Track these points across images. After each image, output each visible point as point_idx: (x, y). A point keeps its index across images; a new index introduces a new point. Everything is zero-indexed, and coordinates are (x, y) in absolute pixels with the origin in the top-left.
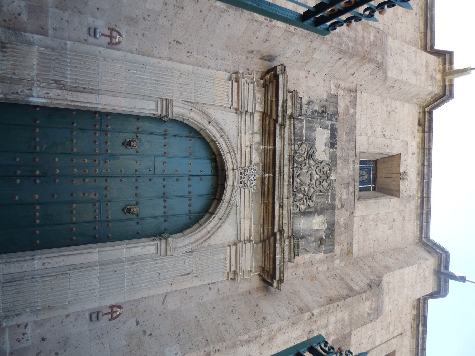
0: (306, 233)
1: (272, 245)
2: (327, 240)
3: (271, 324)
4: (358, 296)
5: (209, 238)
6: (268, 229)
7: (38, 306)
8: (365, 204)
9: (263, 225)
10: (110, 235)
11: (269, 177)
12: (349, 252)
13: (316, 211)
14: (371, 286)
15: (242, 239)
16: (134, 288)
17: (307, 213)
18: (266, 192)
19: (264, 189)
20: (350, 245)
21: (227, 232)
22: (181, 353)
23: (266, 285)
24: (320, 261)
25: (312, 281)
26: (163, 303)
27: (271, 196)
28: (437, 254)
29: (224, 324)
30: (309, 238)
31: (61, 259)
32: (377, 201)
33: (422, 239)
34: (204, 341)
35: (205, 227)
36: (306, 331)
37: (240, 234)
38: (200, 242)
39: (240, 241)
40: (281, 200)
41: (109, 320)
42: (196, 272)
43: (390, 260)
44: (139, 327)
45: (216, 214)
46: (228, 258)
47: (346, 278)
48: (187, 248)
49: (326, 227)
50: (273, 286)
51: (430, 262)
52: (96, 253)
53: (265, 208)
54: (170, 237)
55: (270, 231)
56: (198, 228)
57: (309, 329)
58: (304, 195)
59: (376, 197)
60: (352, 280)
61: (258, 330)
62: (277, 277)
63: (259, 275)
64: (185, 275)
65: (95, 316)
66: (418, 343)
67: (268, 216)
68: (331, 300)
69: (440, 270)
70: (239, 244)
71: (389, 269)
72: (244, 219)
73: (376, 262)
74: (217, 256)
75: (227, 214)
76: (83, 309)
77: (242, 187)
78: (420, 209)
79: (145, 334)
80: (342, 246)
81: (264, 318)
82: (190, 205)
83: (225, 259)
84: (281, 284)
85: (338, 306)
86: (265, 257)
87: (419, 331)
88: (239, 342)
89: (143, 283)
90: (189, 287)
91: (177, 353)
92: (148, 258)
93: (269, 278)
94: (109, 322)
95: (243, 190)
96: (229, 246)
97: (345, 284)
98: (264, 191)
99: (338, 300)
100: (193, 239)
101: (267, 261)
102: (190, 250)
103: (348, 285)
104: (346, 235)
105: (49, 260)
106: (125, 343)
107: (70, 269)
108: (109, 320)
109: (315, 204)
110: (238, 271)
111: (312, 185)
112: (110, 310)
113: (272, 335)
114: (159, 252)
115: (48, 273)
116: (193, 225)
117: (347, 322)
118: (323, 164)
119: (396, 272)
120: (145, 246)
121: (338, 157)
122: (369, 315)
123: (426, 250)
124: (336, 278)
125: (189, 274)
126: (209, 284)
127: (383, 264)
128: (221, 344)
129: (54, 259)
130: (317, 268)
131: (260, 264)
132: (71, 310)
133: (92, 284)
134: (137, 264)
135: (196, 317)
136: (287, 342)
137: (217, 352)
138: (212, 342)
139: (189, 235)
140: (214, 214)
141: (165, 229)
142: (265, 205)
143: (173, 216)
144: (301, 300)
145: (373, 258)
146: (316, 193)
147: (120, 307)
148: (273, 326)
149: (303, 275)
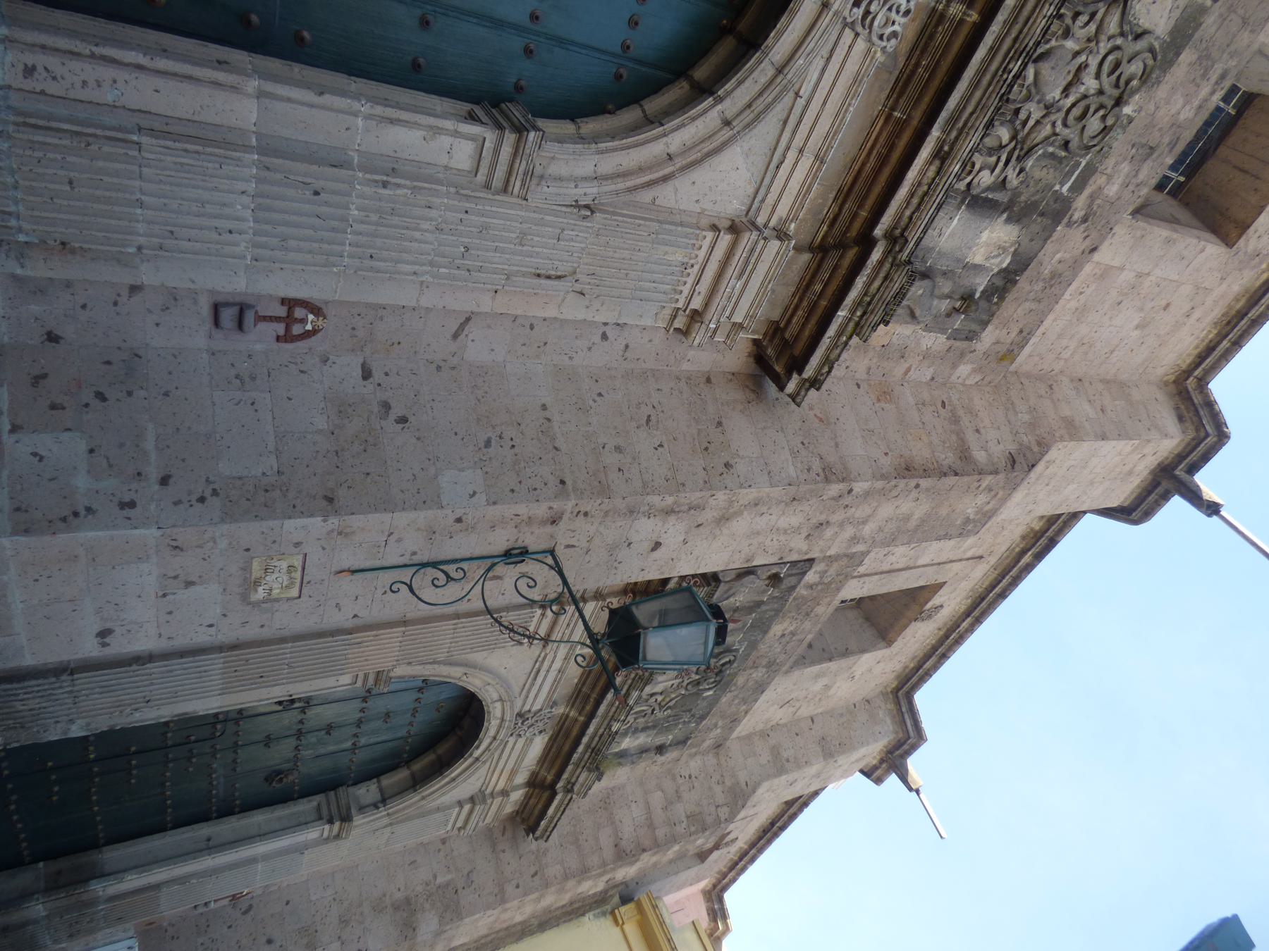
0: (942, 265)
1: (842, 271)
2: (976, 305)
3: (741, 486)
4: (977, 477)
5: (665, 179)
6: (855, 215)
7: (20, 230)
8: (1139, 233)
9: (844, 195)
10: (306, 34)
11: (962, 21)
12: (1009, 355)
13: (1008, 207)
14: (1014, 461)
15: (760, 220)
16: (372, 269)
17: (981, 204)
18: (916, 79)
19: (917, 65)
20: (1025, 336)
21: (726, 182)
22: (484, 498)
23: (758, 371)
24: (927, 356)
25: (879, 400)
26: (455, 336)
27: (927, 99)
28: (1197, 430)
29: (618, 449)
30: (940, 281)
31: (107, 73)
32: (1175, 236)
33: (1187, 379)
34: (553, 481)
35: (665, 135)
36: (814, 521)
37: (763, 201)
38: (630, 184)
39: (753, 224)
40: (954, 134)
41: (278, 339)
42: (583, 278)
43: (1087, 407)
44: (370, 386)
45: (720, 100)
46: (696, 267)
47: (965, 420)
48: (580, 191)
49: (1004, 265)
50: (782, 388)
51: (1168, 440)
52: (248, 95)
53: (882, 140)
54: (536, 129)
55: (857, 225)
56: (635, 129)
57: (823, 518)
58: (1013, 138)
59: (1172, 221)
60: (978, 431)
61: (703, 493)
62: (809, 372)
63: (755, 342)
64: (549, 277)
65: (232, 314)
66: (1000, 581)
67: (878, 171)
68: (907, 469)
69: (1174, 469)
70: (747, 235)
71: (1073, 431)
72: (801, 151)
73: (1053, 401)
74: (667, 248)
75: (754, 113)
76: (192, 286)
77: (852, 25)
78: (1248, 300)
79: (387, 413)
80: (1005, 331)
81: (727, 465)
82: (633, 23)
83: (685, 266)
84: (808, 390)
85: (917, 486)
86: (801, 300)
87: (1018, 561)
88: (647, 508)
89: (408, 263)
90: (546, 315)
91: (475, 493)
92: (439, 182)
93: (783, 360)
94: (275, 346)
95: (848, 35)
96: (714, 228)
97: (958, 435)
98: (913, 72)
99: (926, 473)
100: (610, 163)
101: (800, 313)
102: (587, 201)
103: (962, 440)
104: (1033, 306)
105: (52, 62)
106: (321, 423)
107: (140, 129)
108: (278, 339)
109: (1022, 182)
110: (708, 316)
111: (1059, 110)
112: (282, 311)
113: (731, 510)
114: (483, 170)
115: (50, 117)
116: (620, 107)
117: (913, 523)
118: (1142, 44)
119: (1085, 444)
120: (438, 131)
121: (1197, 36)
122: (968, 520)
123: (1177, 408)
124: (942, 411)
125: (559, 277)
126: (606, 324)
127: (1066, 412)
128: (599, 501)
129: (75, 65)
130: (909, 370)
131: (776, 316)
132: (147, 275)
133: (227, 211)
134: (399, 192)
135: (544, 407)
136: (758, 533)
137: (581, 516)
138: (575, 489)
139: (603, 145)
140: (711, 93)
141: (519, 88)
142: (889, 128)
143: (561, 42)
144: (837, 445)
145: (1051, 387)
146: (1052, 144)
147: (317, 311)
148: (744, 491)
149: (864, 376)
